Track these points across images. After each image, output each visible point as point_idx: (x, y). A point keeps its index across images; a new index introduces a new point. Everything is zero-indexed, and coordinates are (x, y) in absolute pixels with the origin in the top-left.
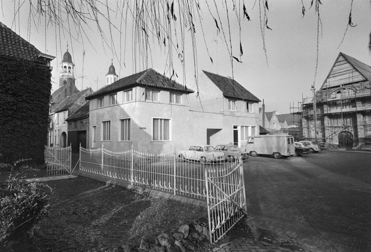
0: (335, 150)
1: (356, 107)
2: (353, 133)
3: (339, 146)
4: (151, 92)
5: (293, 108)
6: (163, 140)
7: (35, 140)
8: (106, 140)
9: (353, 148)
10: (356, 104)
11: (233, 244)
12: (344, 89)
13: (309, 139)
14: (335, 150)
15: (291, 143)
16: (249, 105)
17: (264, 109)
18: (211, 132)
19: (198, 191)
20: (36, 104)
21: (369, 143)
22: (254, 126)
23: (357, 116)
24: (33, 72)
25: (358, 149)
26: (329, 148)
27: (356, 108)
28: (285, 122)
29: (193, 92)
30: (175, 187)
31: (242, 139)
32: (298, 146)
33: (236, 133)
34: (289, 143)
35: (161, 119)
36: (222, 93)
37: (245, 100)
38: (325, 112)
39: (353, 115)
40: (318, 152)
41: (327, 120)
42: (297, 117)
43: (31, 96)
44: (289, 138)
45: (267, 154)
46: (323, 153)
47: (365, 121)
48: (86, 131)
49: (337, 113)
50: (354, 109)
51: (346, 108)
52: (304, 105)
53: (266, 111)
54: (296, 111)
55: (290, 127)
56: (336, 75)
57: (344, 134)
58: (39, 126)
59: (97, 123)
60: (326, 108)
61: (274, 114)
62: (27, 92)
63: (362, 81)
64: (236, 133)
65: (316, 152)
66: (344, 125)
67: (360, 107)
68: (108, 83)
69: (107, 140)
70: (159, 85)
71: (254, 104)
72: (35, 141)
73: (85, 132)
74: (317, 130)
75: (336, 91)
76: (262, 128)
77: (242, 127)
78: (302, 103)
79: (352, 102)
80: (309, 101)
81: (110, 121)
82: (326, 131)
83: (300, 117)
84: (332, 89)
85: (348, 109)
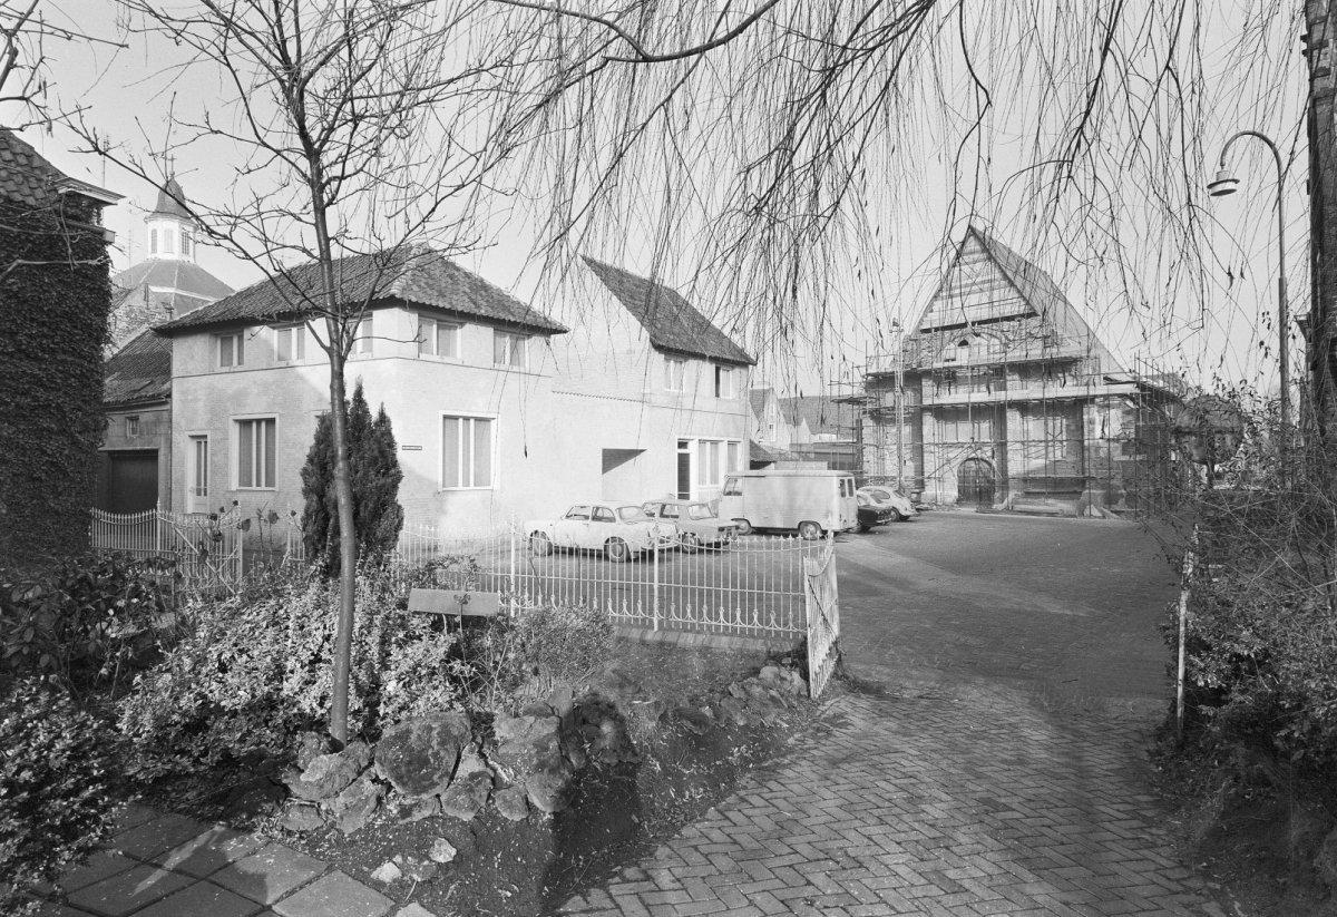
0: (951, 512)
1: (1005, 389)
2: (994, 463)
3: (959, 501)
4: (435, 326)
6: (263, 487)
7: (60, 489)
9: (994, 506)
10: (1005, 381)
12: (978, 335)
13: (882, 480)
14: (951, 512)
15: (847, 494)
16: (722, 373)
18: (613, 458)
19: (722, 616)
20: (63, 362)
22: (733, 439)
23: (1008, 414)
24: (50, 248)
25: (1008, 510)
28: (804, 423)
29: (565, 332)
30: (656, 611)
31: (701, 481)
32: (863, 503)
33: (683, 462)
34: (843, 495)
35: (467, 419)
36: (646, 334)
37: (713, 359)
38: (927, 402)
40: (911, 518)
42: (850, 414)
43: (45, 336)
44: (843, 481)
45: (782, 526)
46: (923, 521)
47: (1026, 428)
48: (155, 452)
50: (1001, 396)
51: (979, 391)
52: (868, 375)
54: (847, 391)
55: (816, 439)
58: (75, 443)
59: (210, 422)
60: (928, 387)
62: (32, 320)
63: (1022, 316)
64: (683, 462)
65: (904, 519)
66: (973, 438)
67: (1017, 390)
68: (154, 250)
69: (258, 485)
70: (463, 305)
71: (737, 370)
72: (60, 494)
73: (152, 456)
74: (904, 451)
76: (756, 445)
77: (702, 442)
78: (863, 371)
80: (885, 366)
81: (270, 422)
82: (926, 456)
83: (856, 412)
84: (947, 334)
85: (980, 396)
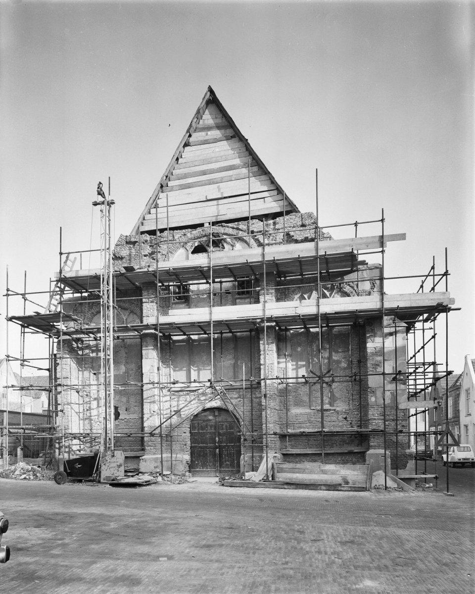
21: (292, 455)
39: (243, 340)
49: (230, 265)
57: (211, 418)
67: (270, 307)
75: (190, 244)
84: (178, 234)
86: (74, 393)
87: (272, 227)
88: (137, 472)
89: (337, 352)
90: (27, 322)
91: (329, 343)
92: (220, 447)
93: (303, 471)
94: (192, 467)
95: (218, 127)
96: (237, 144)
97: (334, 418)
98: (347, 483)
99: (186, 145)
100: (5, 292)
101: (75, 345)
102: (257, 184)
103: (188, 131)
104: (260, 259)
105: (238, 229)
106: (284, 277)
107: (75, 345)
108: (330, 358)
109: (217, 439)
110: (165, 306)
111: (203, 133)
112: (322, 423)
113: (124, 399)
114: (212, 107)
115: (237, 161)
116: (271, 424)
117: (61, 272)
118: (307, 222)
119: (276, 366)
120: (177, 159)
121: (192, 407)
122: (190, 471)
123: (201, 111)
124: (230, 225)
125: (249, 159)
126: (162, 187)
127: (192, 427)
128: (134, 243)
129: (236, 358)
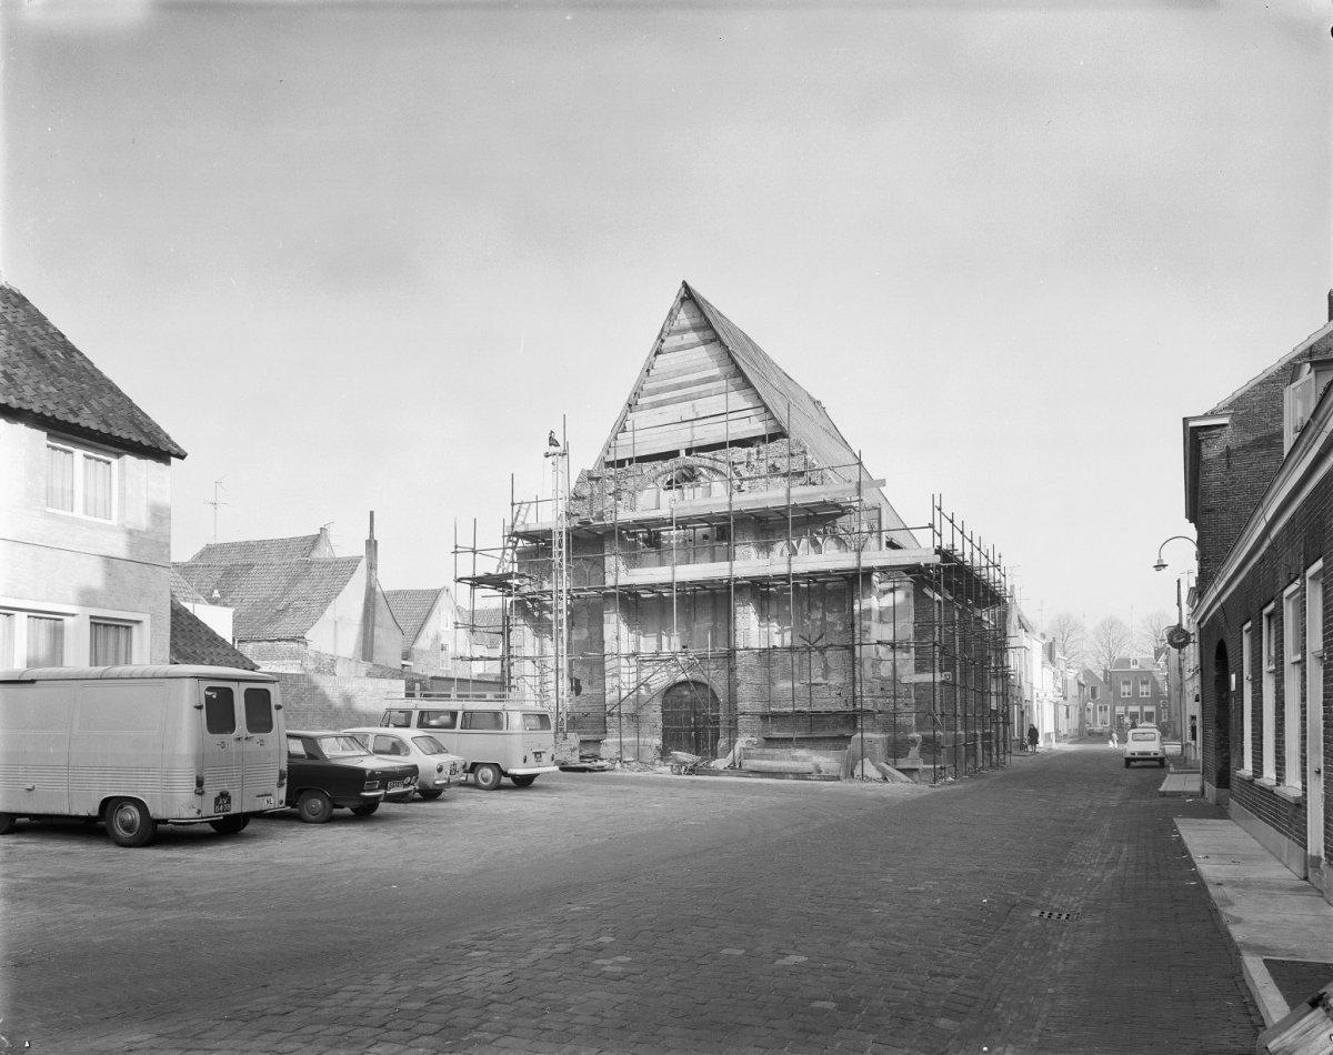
5: (475, 552)
8: (505, 727)
11: (983, 565)
17: (372, 567)
26: (618, 765)
27: (728, 563)
39: (714, 600)
41: (615, 629)
44: (227, 694)
53: (388, 581)
54: (488, 566)
56: (664, 396)
61: (443, 601)
63: (762, 439)
67: (749, 562)
75: (661, 479)
79: (723, 530)
84: (647, 467)
86: (528, 663)
87: (756, 456)
88: (596, 757)
89: (831, 612)
90: (477, 582)
91: (823, 600)
92: (695, 729)
93: (772, 758)
94: (664, 753)
95: (695, 329)
96: (715, 349)
97: (826, 695)
98: (820, 772)
99: (658, 353)
100: (453, 550)
101: (529, 605)
102: (738, 400)
103: (660, 337)
104: (727, 510)
105: (715, 459)
106: (765, 526)
107: (529, 605)
108: (823, 619)
109: (693, 719)
110: (633, 560)
111: (678, 337)
112: (811, 699)
113: (587, 670)
114: (688, 305)
115: (716, 372)
116: (748, 700)
117: (513, 526)
118: (795, 451)
119: (752, 629)
120: (648, 371)
121: (661, 679)
122: (662, 759)
123: (675, 312)
124: (706, 454)
125: (731, 368)
126: (630, 405)
127: (664, 705)
128: (597, 479)
129: (715, 620)
